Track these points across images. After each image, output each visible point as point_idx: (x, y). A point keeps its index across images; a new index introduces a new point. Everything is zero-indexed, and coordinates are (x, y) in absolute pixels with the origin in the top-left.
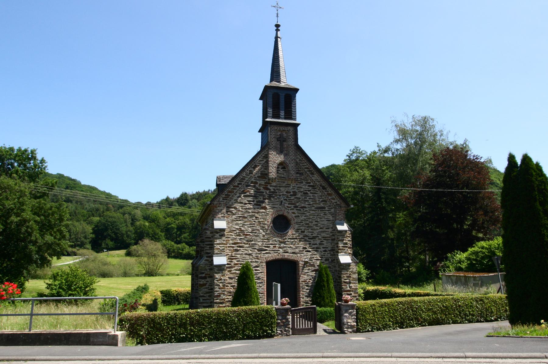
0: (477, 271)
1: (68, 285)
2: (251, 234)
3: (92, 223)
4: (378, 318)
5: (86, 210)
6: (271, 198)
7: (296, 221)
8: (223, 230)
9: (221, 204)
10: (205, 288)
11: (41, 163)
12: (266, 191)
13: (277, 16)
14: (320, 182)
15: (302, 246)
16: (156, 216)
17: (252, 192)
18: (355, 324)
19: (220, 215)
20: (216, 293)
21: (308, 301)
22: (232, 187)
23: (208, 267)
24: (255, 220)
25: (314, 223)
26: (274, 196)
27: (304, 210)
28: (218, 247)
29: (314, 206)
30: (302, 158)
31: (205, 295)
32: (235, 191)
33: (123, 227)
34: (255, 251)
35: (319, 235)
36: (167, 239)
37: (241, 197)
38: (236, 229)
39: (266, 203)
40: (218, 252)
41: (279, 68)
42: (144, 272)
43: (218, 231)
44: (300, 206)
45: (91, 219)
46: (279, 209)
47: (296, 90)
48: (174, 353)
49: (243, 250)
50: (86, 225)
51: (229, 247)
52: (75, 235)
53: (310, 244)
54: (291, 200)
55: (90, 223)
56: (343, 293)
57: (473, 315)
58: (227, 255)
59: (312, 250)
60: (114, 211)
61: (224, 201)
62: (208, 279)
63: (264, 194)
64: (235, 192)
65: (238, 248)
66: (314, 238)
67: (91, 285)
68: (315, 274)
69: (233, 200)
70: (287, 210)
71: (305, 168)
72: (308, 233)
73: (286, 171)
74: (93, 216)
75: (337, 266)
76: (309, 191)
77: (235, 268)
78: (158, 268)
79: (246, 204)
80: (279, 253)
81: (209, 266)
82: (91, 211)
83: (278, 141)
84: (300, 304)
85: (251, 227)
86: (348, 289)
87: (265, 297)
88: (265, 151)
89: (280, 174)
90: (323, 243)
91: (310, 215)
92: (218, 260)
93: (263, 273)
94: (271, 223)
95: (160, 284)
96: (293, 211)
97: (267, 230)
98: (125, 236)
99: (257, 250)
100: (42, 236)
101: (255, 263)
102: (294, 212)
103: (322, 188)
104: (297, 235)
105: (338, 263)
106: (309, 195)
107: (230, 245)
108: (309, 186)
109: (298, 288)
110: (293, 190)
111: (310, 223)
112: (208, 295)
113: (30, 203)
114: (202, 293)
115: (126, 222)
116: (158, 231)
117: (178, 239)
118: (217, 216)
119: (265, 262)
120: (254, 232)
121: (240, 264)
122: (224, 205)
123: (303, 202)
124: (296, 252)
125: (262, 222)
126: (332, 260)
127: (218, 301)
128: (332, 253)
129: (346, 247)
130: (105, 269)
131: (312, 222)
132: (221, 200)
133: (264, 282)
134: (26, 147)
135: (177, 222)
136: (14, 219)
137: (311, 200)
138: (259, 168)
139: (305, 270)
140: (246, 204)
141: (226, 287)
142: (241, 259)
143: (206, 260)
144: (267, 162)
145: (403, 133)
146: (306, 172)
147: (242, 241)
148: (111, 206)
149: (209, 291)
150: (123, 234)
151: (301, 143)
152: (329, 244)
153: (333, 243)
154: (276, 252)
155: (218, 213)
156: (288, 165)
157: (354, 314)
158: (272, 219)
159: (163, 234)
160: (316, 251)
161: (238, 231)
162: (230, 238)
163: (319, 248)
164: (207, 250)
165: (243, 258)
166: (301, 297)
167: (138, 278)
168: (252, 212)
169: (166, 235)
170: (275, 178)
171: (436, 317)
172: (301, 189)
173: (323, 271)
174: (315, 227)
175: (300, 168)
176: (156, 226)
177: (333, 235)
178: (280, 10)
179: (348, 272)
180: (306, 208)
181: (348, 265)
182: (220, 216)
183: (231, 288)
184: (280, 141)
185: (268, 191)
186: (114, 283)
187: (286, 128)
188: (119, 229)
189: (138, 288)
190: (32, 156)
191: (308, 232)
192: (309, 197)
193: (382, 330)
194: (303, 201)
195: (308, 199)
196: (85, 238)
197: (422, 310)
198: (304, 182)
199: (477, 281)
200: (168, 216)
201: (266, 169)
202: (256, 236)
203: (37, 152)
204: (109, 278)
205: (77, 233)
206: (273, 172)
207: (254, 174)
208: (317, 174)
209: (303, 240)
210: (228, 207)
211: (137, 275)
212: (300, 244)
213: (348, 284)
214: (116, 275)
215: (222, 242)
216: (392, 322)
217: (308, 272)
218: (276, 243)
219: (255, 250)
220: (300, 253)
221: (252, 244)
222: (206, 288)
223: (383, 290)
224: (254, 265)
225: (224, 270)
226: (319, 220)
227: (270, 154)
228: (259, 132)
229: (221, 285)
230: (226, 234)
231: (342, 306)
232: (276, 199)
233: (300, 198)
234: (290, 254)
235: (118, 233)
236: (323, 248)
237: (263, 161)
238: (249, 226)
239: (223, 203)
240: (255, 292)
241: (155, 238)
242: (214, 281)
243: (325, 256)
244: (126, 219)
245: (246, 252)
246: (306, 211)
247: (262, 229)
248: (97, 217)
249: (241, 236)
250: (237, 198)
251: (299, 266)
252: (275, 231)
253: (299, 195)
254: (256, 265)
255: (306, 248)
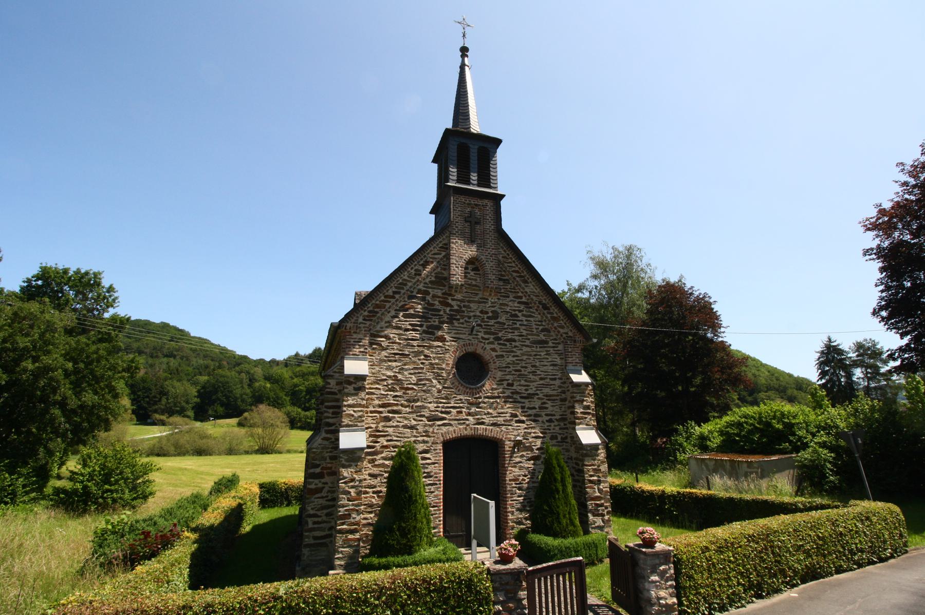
0: (742, 452)
1: (104, 475)
2: (415, 387)
3: (198, 383)
4: (719, 580)
5: (192, 367)
6: (454, 321)
7: (497, 364)
8: (362, 378)
9: (360, 328)
10: (319, 498)
11: (108, 291)
12: (445, 308)
14: (538, 296)
15: (510, 410)
16: (280, 376)
17: (419, 308)
18: (675, 600)
19: (357, 350)
20: (342, 511)
21: (521, 518)
22: (383, 298)
23: (327, 452)
24: (424, 361)
25: (530, 369)
26: (458, 317)
27: (511, 344)
28: (350, 411)
29: (529, 339)
30: (508, 255)
31: (319, 513)
32: (388, 305)
33: (238, 389)
34: (422, 421)
35: (538, 392)
36: (293, 404)
37: (398, 317)
38: (387, 376)
39: (444, 329)
40: (350, 423)
41: (468, 109)
42: (257, 448)
43: (352, 380)
44: (505, 338)
45: (197, 379)
46: (468, 342)
47: (497, 142)
49: (398, 419)
50: (189, 386)
51: (372, 412)
52: (174, 398)
53: (523, 408)
54: (489, 325)
55: (195, 384)
56: (589, 503)
57: (862, 551)
58: (367, 428)
59: (527, 420)
60: (228, 369)
61: (365, 324)
62: (327, 479)
63: (442, 313)
64: (386, 308)
65: (391, 415)
66: (530, 396)
67: (146, 474)
68: (533, 464)
69: (384, 321)
70: (482, 344)
71: (513, 271)
72: (520, 388)
73: (479, 274)
74: (201, 375)
75: (572, 449)
76: (520, 311)
77: (383, 455)
78: (275, 443)
79: (407, 330)
80: (468, 425)
81: (331, 452)
82: (198, 369)
83: (466, 221)
84: (507, 526)
85: (415, 373)
86: (596, 495)
87: (440, 514)
88: (444, 237)
89: (470, 279)
90: (547, 406)
91: (523, 355)
92: (350, 440)
93: (436, 465)
94: (452, 368)
95: (272, 467)
96: (492, 346)
97: (446, 380)
98: (240, 400)
99: (427, 418)
100: (78, 394)
101: (422, 445)
102: (494, 348)
103: (543, 307)
104: (501, 390)
105: (574, 444)
106: (520, 319)
107: (374, 407)
108: (519, 303)
109: (501, 492)
110: (493, 309)
111: (522, 369)
112: (325, 511)
113: (63, 342)
114: (312, 509)
115: (241, 382)
116: (282, 394)
117: (307, 405)
118: (351, 351)
119: (442, 442)
120: (420, 384)
121: (394, 447)
122: (365, 331)
123: (511, 331)
124: (499, 422)
125: (437, 364)
126: (562, 438)
127: (345, 527)
128: (562, 424)
129: (589, 413)
130: (202, 443)
131: (526, 367)
132: (361, 320)
133: (438, 482)
134: (88, 269)
135: (307, 383)
136: (29, 365)
137: (524, 327)
138: (432, 265)
139: (516, 457)
140: (407, 330)
141: (364, 494)
142: (395, 436)
143: (324, 439)
144: (448, 257)
145: (603, 266)
146: (514, 278)
147: (397, 401)
148: (225, 363)
149: (328, 503)
150: (236, 399)
151: (506, 226)
152: (557, 409)
153: (563, 406)
154: (462, 422)
155: (353, 345)
156: (485, 264)
157: (671, 576)
158: (454, 359)
159: (288, 399)
160: (534, 421)
161: (390, 382)
162: (374, 394)
163: (539, 416)
164: (328, 418)
165: (400, 435)
166: (509, 512)
167: (247, 456)
168: (418, 346)
169: (291, 399)
170: (462, 285)
171: (810, 564)
172: (506, 307)
173: (555, 462)
174: (531, 376)
175: (504, 271)
176: (279, 388)
177: (564, 392)
179: (596, 462)
180: (514, 341)
181: (595, 447)
182: (358, 350)
183: (374, 497)
184: (470, 222)
185: (448, 309)
186: (207, 465)
187: (480, 202)
188: (231, 392)
189: (220, 480)
190: (95, 282)
191: (520, 385)
192: (520, 323)
193: (728, 610)
194: (511, 329)
195: (518, 326)
196: (187, 403)
197: (788, 551)
198: (511, 296)
199: (755, 468)
200: (297, 377)
201: (445, 269)
202: (424, 391)
203: (102, 276)
204: (206, 457)
205: (177, 397)
206: (457, 274)
207: (423, 276)
208: (533, 283)
209: (510, 400)
210: (374, 336)
211: (247, 453)
212: (505, 407)
213: (595, 484)
214: (217, 452)
215: (360, 401)
216: (743, 585)
217: (521, 462)
218: (461, 405)
219: (424, 419)
220: (506, 425)
221: (416, 407)
222: (322, 497)
223: (618, 485)
224: (420, 449)
225: (360, 459)
226: (537, 364)
227: (453, 243)
228: (431, 213)
229: (352, 491)
230: (367, 386)
231: (642, 556)
232: (462, 324)
233: (505, 324)
234: (487, 427)
235: (230, 397)
236: (547, 415)
237: (440, 254)
238: (412, 371)
239: (364, 327)
240: (424, 508)
241: (276, 403)
242: (338, 482)
243: (550, 430)
244: (242, 379)
245: (406, 422)
246: (515, 347)
247: (436, 379)
248: (205, 376)
249: (397, 391)
250: (391, 319)
251: (504, 451)
252: (460, 383)
253: (504, 318)
254: (425, 447)
255: (516, 416)
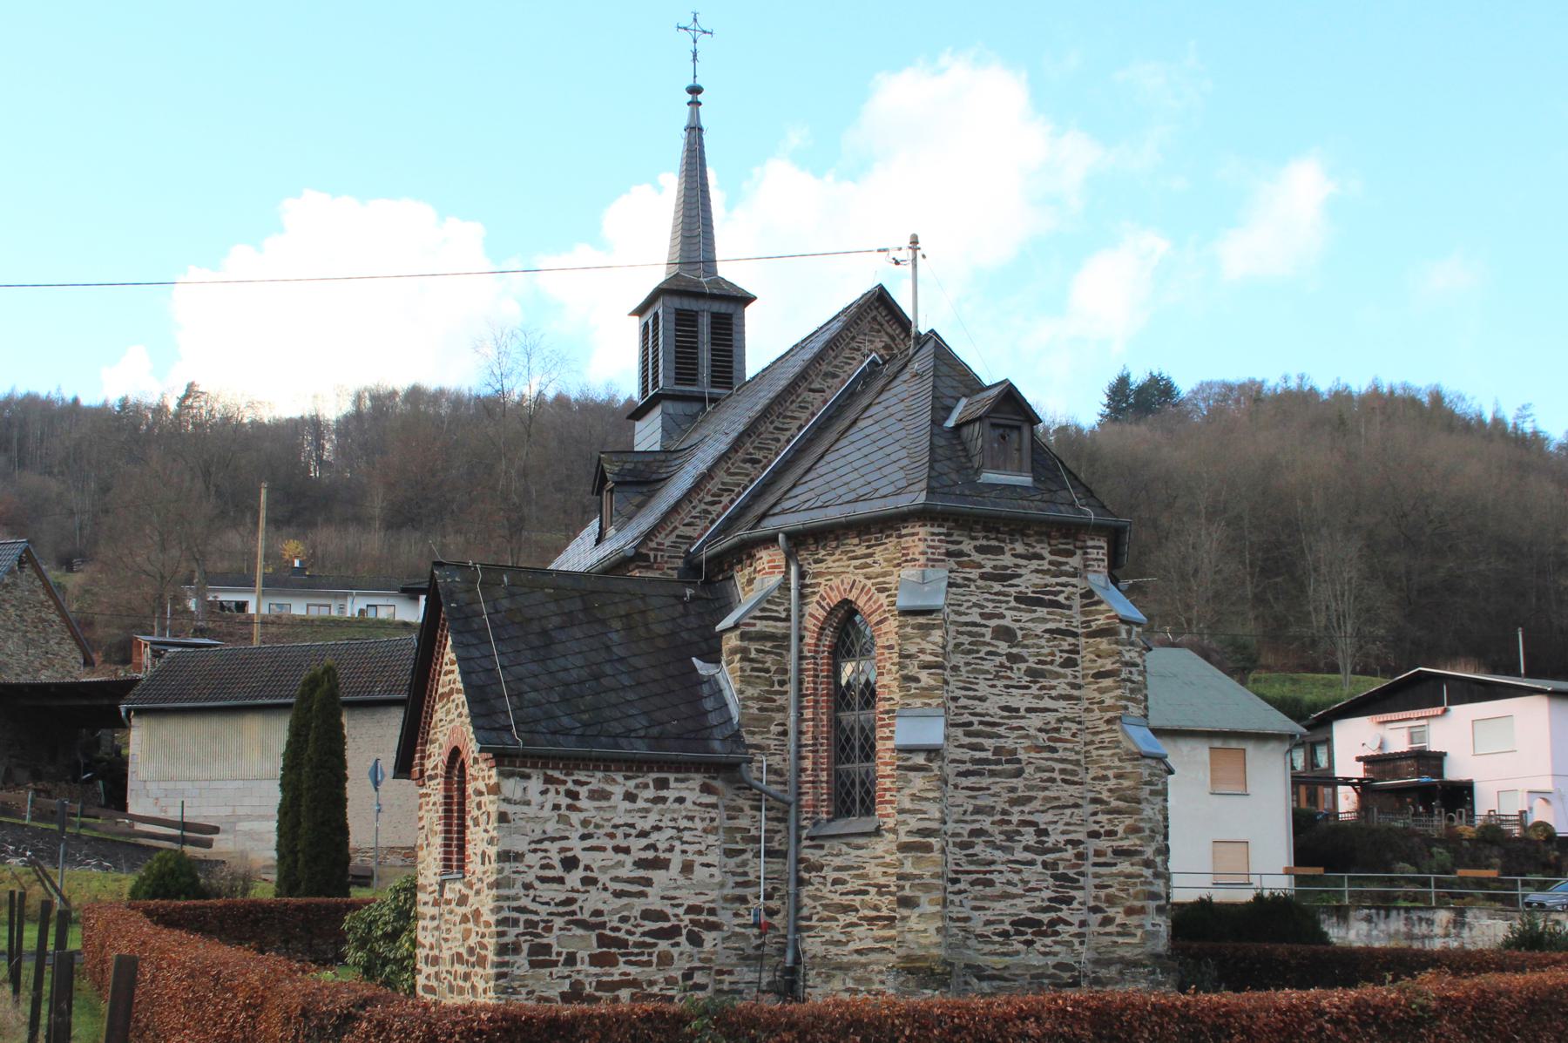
13: (695, 55)
48: (653, 331)
178: (702, 39)
